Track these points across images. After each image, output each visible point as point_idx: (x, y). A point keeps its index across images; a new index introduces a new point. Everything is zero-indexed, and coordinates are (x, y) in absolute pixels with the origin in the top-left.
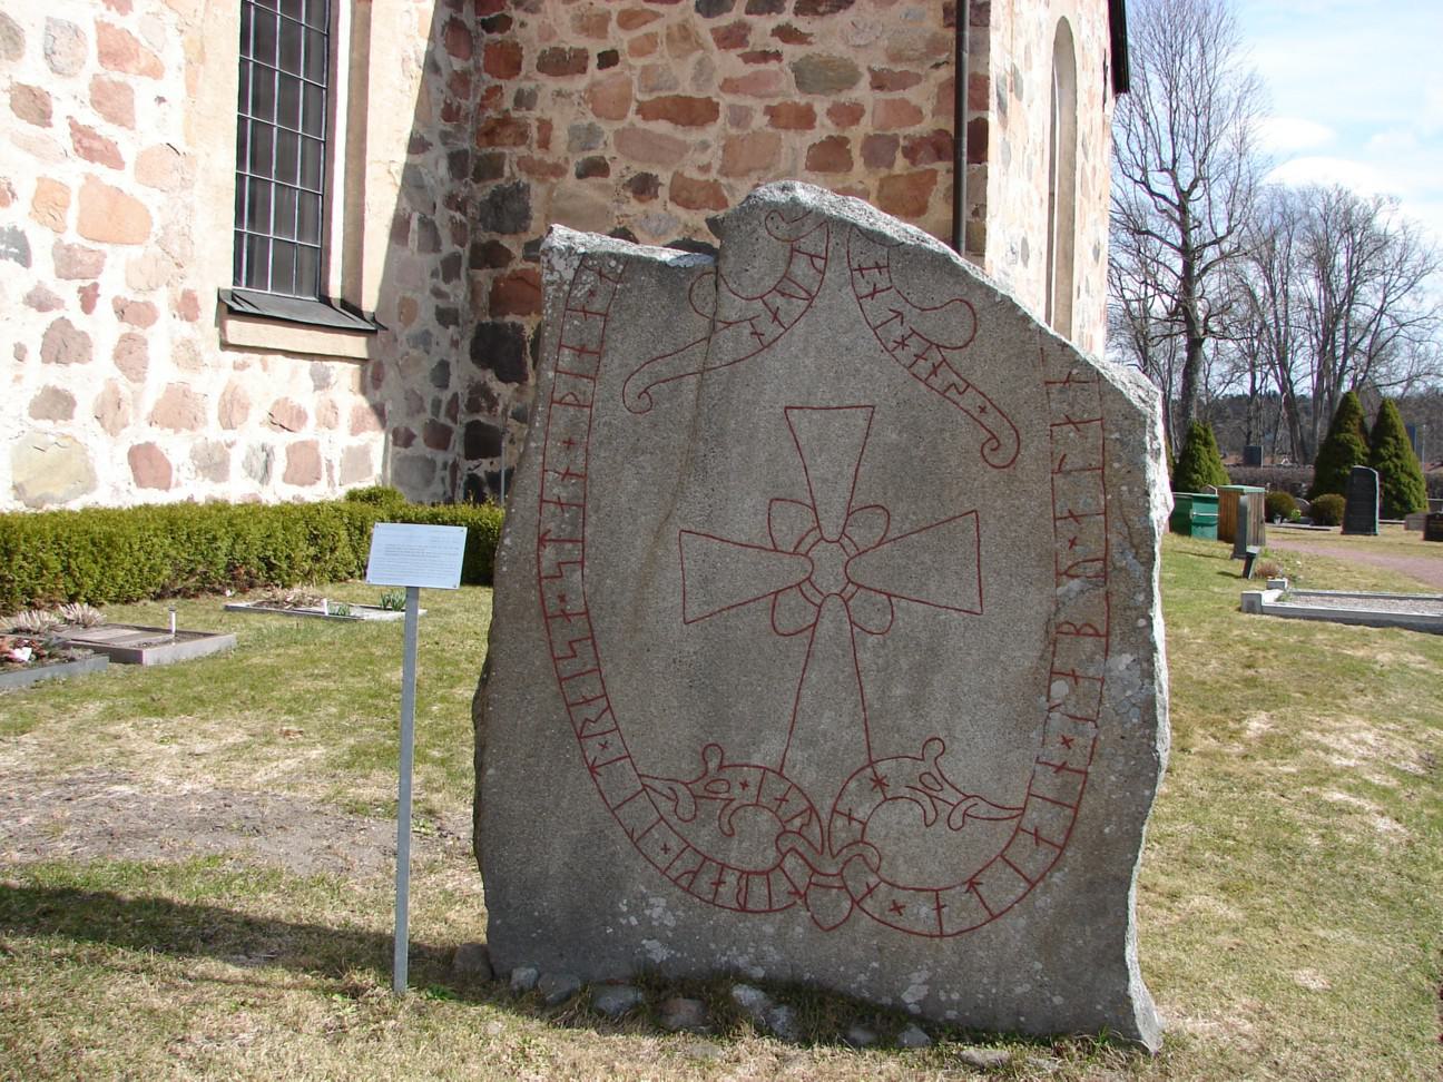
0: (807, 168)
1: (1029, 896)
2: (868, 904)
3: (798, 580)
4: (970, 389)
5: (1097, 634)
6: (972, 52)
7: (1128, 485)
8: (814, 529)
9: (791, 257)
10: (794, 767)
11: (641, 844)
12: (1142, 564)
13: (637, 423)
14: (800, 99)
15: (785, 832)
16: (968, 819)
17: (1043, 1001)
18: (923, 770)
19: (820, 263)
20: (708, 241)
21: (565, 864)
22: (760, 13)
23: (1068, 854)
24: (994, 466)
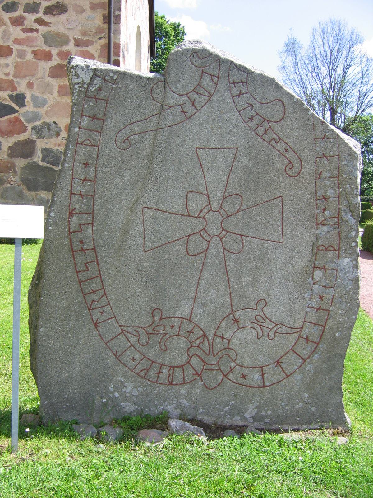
0: (49, 76)
1: (303, 366)
2: (231, 376)
3: (199, 230)
4: (281, 141)
5: (335, 250)
6: (114, 34)
7: (350, 184)
8: (207, 205)
9: (202, 76)
10: (196, 317)
11: (121, 358)
12: (355, 219)
13: (123, 155)
14: (47, 49)
15: (192, 347)
16: (277, 334)
17: (307, 410)
18: (256, 314)
19: (215, 79)
20: (9, 104)
21: (82, 371)
22: (29, 13)
23: (320, 346)
24: (290, 176)
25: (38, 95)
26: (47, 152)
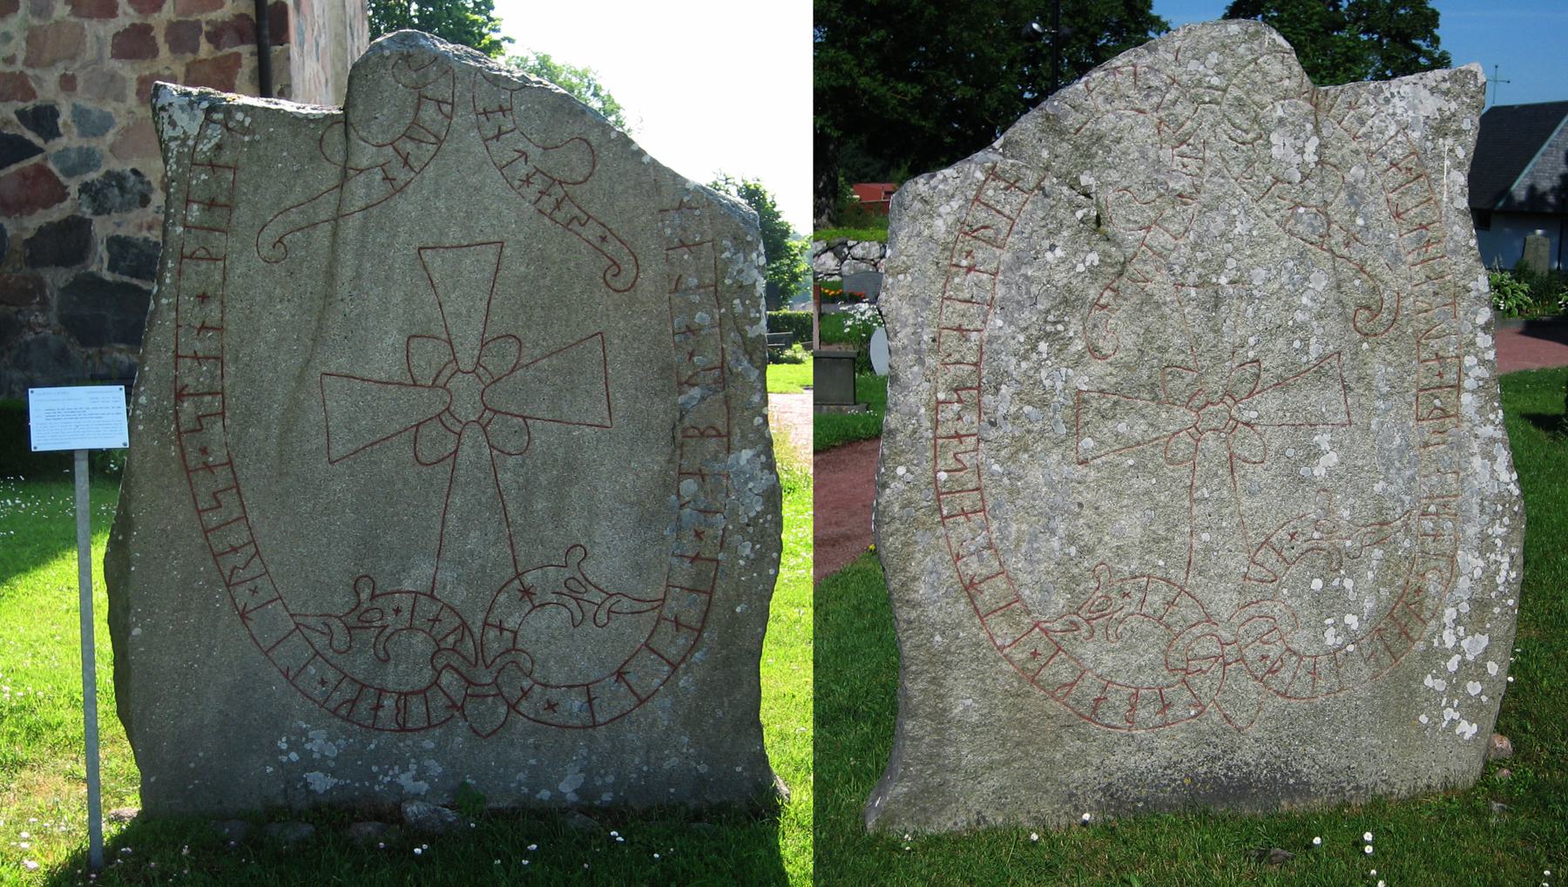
2: (524, 706)
5: (719, 435)
16: (613, 616)
19: (446, 108)
25: (89, 105)
26: (119, 246)
